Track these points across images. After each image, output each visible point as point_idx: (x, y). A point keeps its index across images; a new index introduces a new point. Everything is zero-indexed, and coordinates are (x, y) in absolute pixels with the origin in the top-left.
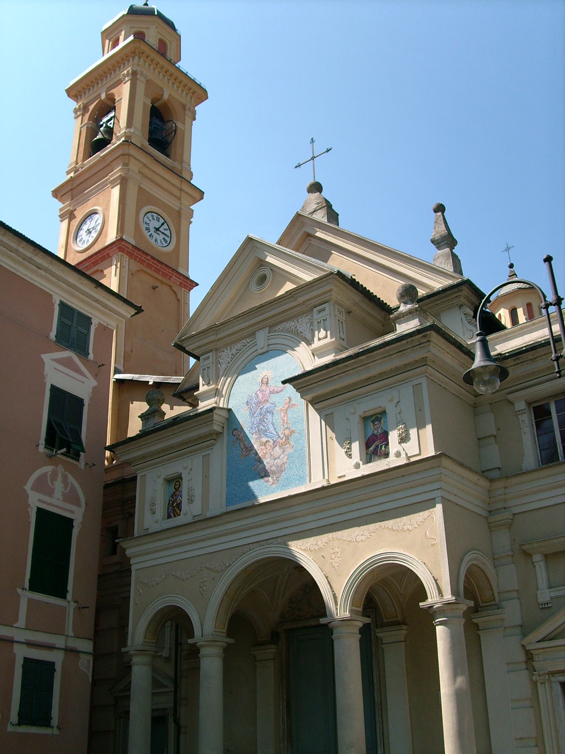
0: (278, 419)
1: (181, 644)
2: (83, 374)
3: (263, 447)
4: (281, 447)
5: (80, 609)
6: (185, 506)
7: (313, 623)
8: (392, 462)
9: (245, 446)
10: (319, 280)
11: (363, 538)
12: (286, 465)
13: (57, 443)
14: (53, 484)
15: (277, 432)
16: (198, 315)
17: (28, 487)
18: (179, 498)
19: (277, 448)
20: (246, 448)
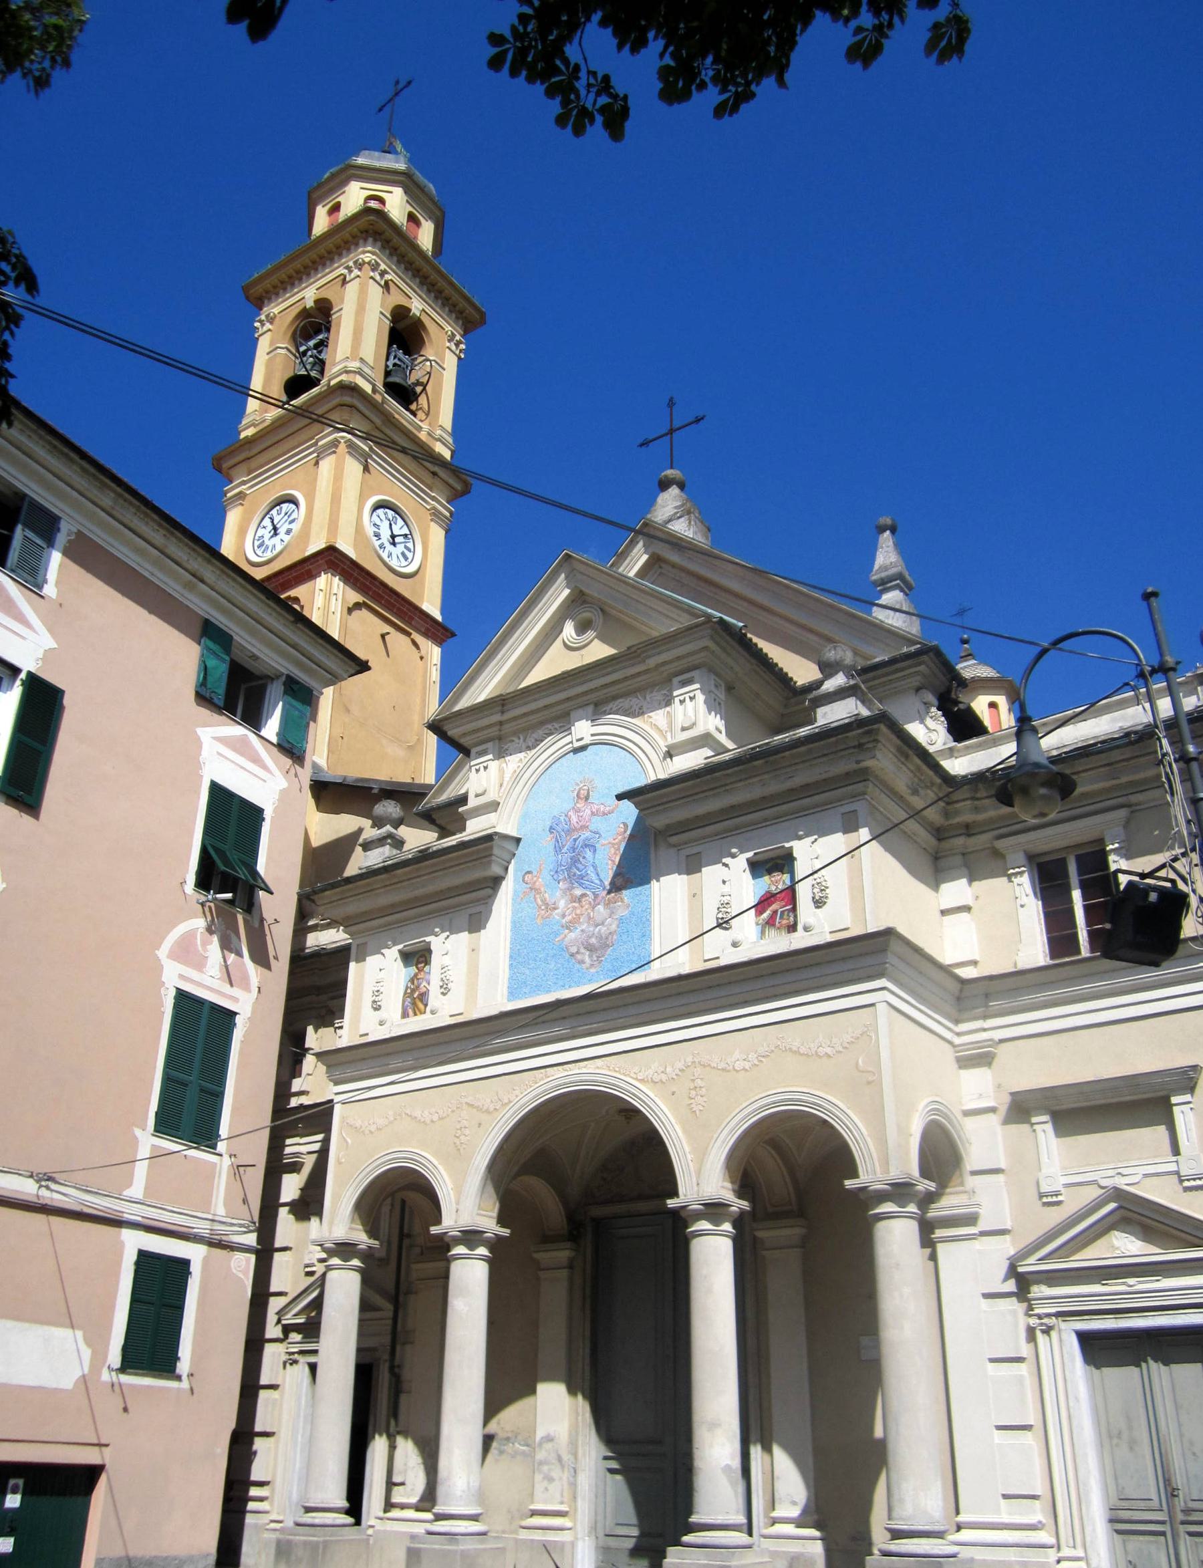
1: (409, 1236)
2: (265, 767)
3: (576, 905)
4: (607, 905)
5: (238, 1169)
6: (435, 999)
7: (643, 1206)
8: (799, 940)
11: (747, 1065)
13: (216, 881)
14: (205, 950)
17: (163, 953)
18: (424, 983)
19: (600, 908)
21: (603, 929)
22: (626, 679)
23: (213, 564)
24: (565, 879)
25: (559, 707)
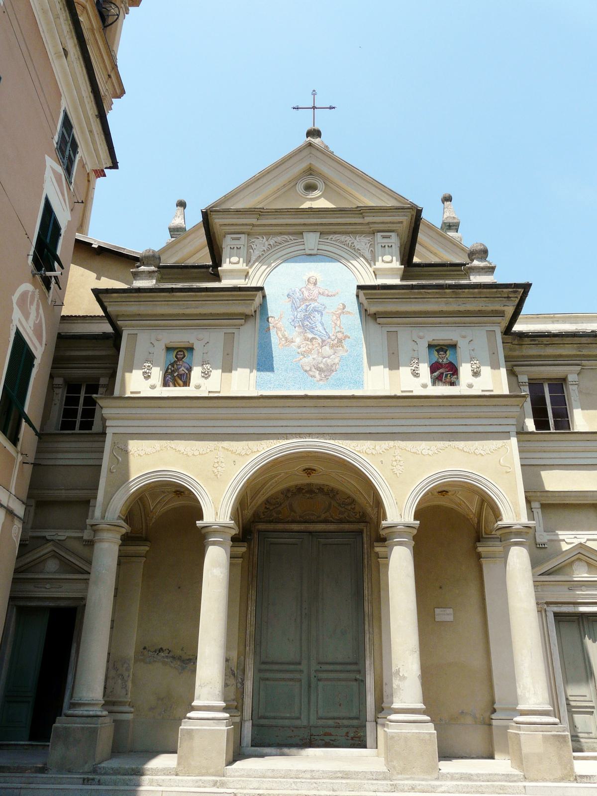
4: (332, 347)
9: (284, 336)
10: (396, 209)
12: (337, 366)
15: (326, 332)
16: (236, 194)
19: (327, 348)
23: (76, 48)
25: (298, 228)
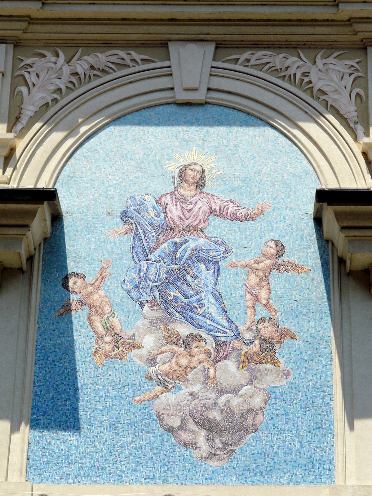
0: (237, 289)
9: (110, 329)
12: (260, 417)
19: (230, 365)
20: (116, 338)
21: (235, 401)
22: (288, 22)
24: (154, 303)
